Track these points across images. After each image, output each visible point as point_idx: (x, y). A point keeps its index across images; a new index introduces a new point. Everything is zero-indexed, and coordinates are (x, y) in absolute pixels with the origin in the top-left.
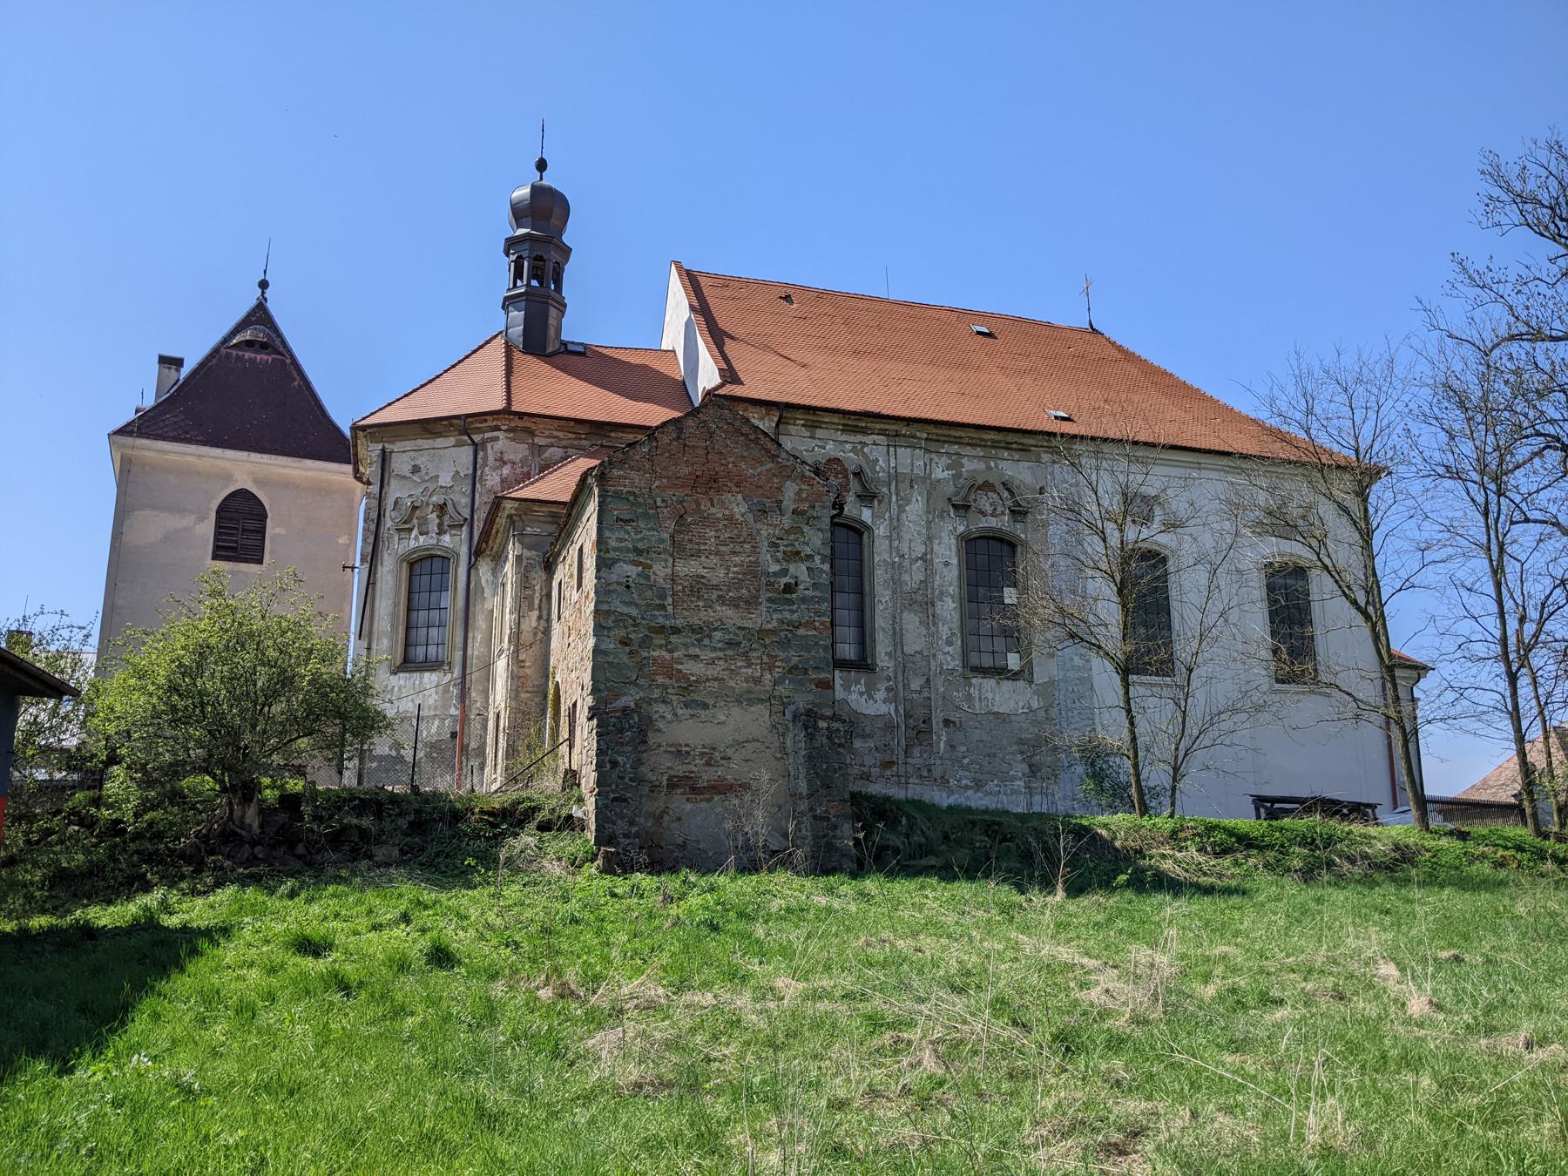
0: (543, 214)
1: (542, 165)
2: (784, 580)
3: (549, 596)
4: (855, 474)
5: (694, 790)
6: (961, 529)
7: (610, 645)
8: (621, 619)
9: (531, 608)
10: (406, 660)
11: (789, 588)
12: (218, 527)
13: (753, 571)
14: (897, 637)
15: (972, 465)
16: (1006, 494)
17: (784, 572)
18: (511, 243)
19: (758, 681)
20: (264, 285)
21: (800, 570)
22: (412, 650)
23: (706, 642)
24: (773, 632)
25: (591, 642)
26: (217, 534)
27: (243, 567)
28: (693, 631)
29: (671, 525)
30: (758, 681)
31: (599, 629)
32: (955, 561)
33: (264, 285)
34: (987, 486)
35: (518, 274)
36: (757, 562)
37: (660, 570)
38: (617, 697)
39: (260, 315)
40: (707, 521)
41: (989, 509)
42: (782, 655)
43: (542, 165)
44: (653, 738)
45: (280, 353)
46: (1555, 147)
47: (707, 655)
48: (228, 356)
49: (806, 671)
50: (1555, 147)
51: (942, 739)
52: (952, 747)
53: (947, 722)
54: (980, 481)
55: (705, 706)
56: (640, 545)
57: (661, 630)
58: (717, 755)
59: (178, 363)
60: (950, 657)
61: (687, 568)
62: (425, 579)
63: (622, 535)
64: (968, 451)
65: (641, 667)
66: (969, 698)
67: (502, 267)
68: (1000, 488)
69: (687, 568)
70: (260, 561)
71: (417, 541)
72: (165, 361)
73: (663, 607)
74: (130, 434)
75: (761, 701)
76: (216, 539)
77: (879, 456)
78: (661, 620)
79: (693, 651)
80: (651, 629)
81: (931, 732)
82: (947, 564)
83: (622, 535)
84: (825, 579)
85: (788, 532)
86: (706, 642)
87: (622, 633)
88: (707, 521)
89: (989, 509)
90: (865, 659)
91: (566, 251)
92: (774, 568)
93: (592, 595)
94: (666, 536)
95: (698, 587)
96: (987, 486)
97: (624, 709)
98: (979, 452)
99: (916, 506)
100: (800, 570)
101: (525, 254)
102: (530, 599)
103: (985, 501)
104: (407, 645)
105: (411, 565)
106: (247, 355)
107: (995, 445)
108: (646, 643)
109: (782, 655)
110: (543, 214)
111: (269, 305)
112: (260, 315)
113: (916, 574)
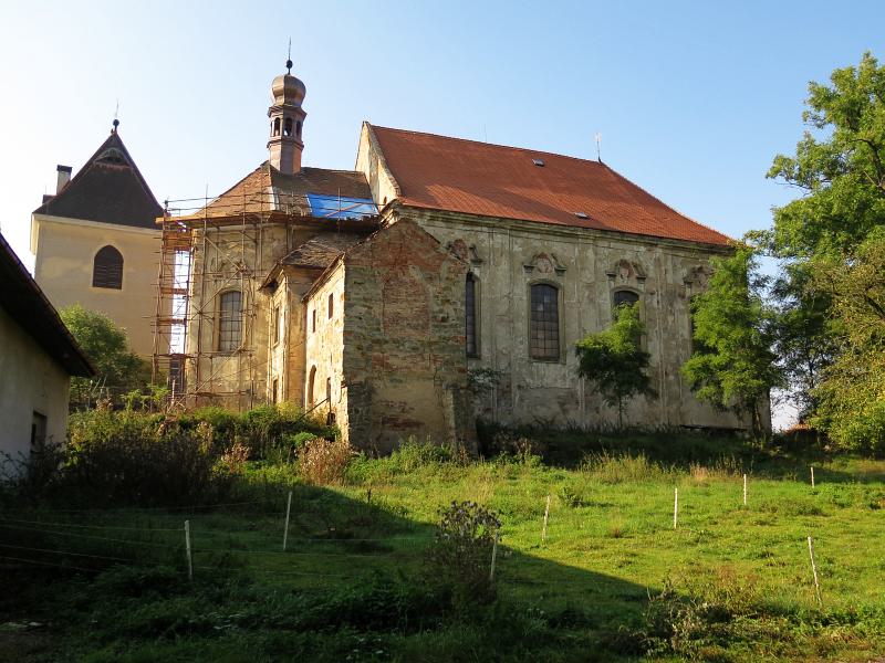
0: (292, 91)
1: (289, 64)
2: (441, 315)
3: (306, 317)
4: (471, 248)
5: (396, 425)
6: (528, 280)
7: (352, 349)
8: (357, 337)
9: (296, 325)
10: (220, 349)
11: (444, 320)
12: (95, 267)
13: (424, 310)
14: (493, 340)
15: (537, 243)
16: (553, 260)
17: (441, 311)
18: (273, 110)
19: (428, 369)
20: (116, 123)
21: (449, 309)
22: (223, 343)
23: (401, 348)
24: (436, 343)
25: (342, 347)
26: (95, 272)
27: (110, 290)
28: (394, 342)
29: (382, 286)
30: (428, 369)
31: (346, 341)
32: (525, 298)
33: (116, 123)
34: (543, 256)
35: (277, 127)
36: (427, 306)
37: (377, 310)
38: (355, 376)
39: (114, 142)
40: (402, 283)
41: (544, 268)
42: (441, 355)
43: (289, 64)
44: (375, 398)
45: (126, 164)
46: (882, 415)
47: (401, 355)
48: (98, 166)
49: (453, 364)
50: (882, 415)
51: (516, 395)
52: (522, 400)
53: (519, 387)
54: (540, 252)
55: (401, 381)
56: (366, 296)
57: (378, 342)
58: (407, 408)
59: (69, 170)
60: (522, 350)
61: (391, 309)
62: (230, 304)
63: (357, 291)
64: (532, 236)
65: (367, 360)
66: (531, 375)
67: (269, 122)
68: (549, 256)
69: (391, 309)
70: (120, 288)
71: (225, 284)
72: (61, 168)
73: (378, 330)
74: (44, 213)
75: (430, 379)
76: (95, 275)
77: (485, 239)
78: (378, 337)
79: (394, 353)
80: (373, 341)
81: (510, 392)
82: (521, 299)
83: (357, 291)
84: (463, 314)
85: (444, 289)
86: (401, 348)
87: (358, 343)
88: (402, 283)
89: (544, 268)
90: (475, 352)
91: (304, 115)
92: (437, 309)
93: (341, 322)
94: (380, 292)
95: (396, 319)
96: (543, 256)
97: (360, 383)
98: (539, 236)
99: (504, 266)
100: (449, 309)
101: (281, 117)
102: (295, 319)
103: (541, 264)
104: (220, 340)
105: (222, 296)
106: (108, 166)
107: (548, 233)
108: (370, 348)
109: (441, 355)
110: (292, 91)
111: (120, 133)
112: (114, 142)
113: (503, 308)
